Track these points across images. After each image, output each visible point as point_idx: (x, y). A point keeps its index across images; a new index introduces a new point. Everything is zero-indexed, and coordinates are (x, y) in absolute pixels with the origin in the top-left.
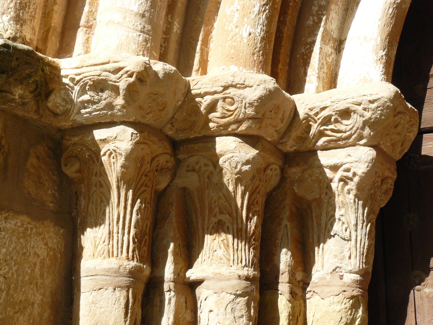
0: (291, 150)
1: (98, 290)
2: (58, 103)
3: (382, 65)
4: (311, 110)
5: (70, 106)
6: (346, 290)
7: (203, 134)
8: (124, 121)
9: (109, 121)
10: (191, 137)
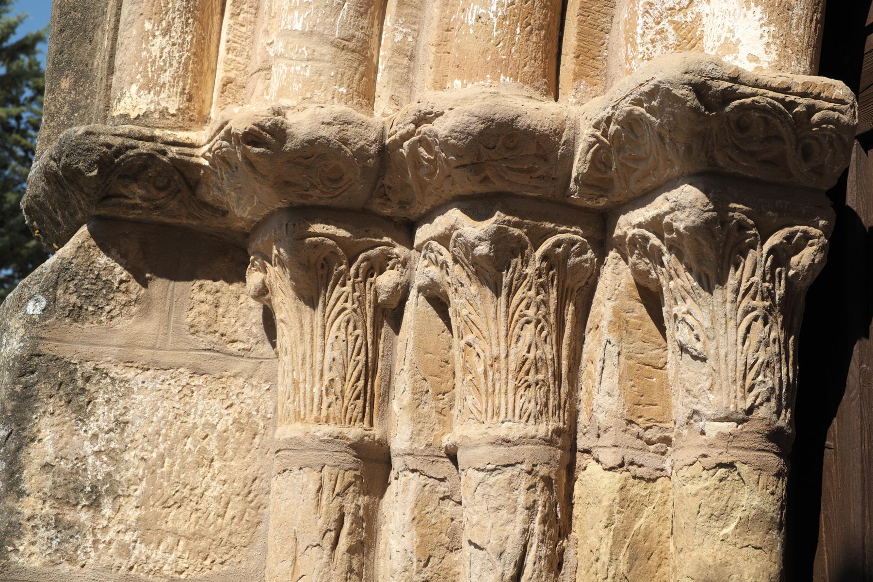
6: (706, 453)
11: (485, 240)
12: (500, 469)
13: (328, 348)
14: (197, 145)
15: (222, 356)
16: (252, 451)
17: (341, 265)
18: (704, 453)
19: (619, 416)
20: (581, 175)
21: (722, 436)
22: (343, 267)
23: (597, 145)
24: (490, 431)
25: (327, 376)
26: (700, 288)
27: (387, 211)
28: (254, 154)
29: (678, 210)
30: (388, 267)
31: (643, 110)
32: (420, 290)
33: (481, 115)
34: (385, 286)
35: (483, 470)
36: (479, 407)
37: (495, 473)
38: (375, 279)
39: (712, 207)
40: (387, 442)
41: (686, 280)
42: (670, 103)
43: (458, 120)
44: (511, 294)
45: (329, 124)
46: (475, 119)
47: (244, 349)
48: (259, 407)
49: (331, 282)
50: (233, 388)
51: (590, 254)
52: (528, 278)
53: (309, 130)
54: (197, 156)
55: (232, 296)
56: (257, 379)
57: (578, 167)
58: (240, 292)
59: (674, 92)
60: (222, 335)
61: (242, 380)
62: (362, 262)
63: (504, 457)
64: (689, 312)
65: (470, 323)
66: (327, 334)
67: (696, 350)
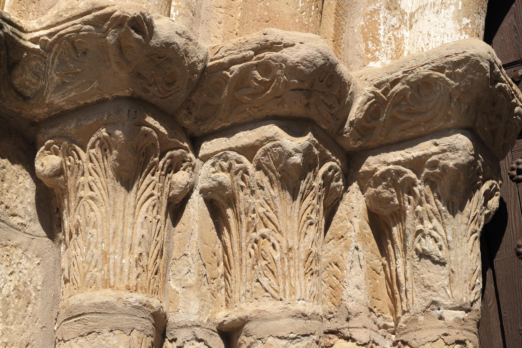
0: (356, 146)
1: (88, 335)
2: (27, 80)
3: (467, 35)
4: (378, 86)
5: (44, 83)
6: (447, 333)
7: (232, 122)
8: (118, 96)
9: (97, 99)
10: (216, 128)
11: (300, 152)
12: (299, 338)
13: (138, 225)
14: (25, 29)
15: (6, 226)
16: (26, 318)
17: (155, 157)
18: (445, 332)
19: (365, 305)
20: (357, 120)
21: (458, 320)
22: (157, 159)
23: (374, 100)
24: (290, 306)
25: (137, 250)
26: (448, 211)
27: (187, 122)
28: (135, 38)
29: (450, 151)
30: (182, 168)
31: (444, 75)
32: (203, 191)
33: (324, 52)
34: (180, 183)
35: (285, 338)
36: (276, 287)
37: (295, 341)
38: (172, 175)
39: (474, 153)
40: (165, 317)
41: (434, 205)
42: (474, 72)
43: (310, 52)
44: (303, 200)
45: (180, 35)
46: (319, 55)
47: (22, 224)
48: (32, 279)
49: (146, 170)
50: (14, 257)
51: (341, 183)
52: (314, 190)
53: (168, 35)
54: (24, 40)
55: (14, 174)
56: (31, 253)
57: (354, 114)
58: (19, 173)
59: (482, 63)
60: (7, 207)
61: (20, 251)
62: (168, 158)
63: (303, 328)
64: (435, 229)
65: (266, 219)
66: (136, 214)
67: (438, 257)
